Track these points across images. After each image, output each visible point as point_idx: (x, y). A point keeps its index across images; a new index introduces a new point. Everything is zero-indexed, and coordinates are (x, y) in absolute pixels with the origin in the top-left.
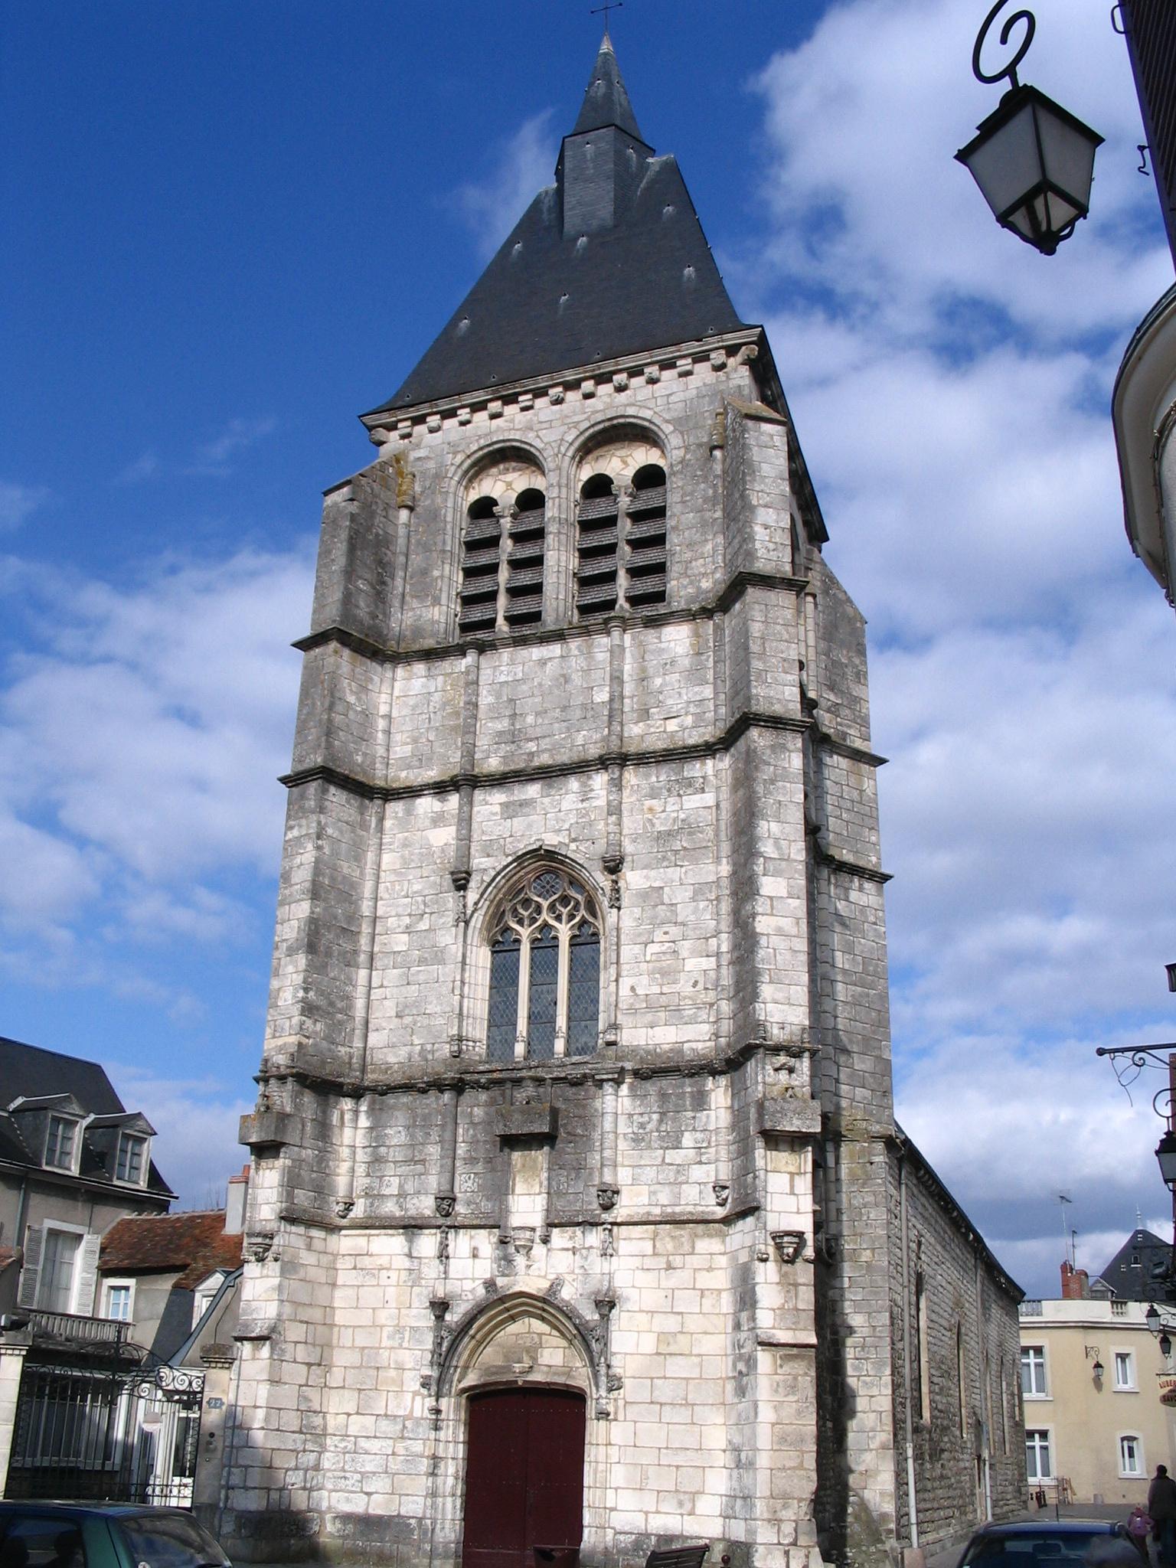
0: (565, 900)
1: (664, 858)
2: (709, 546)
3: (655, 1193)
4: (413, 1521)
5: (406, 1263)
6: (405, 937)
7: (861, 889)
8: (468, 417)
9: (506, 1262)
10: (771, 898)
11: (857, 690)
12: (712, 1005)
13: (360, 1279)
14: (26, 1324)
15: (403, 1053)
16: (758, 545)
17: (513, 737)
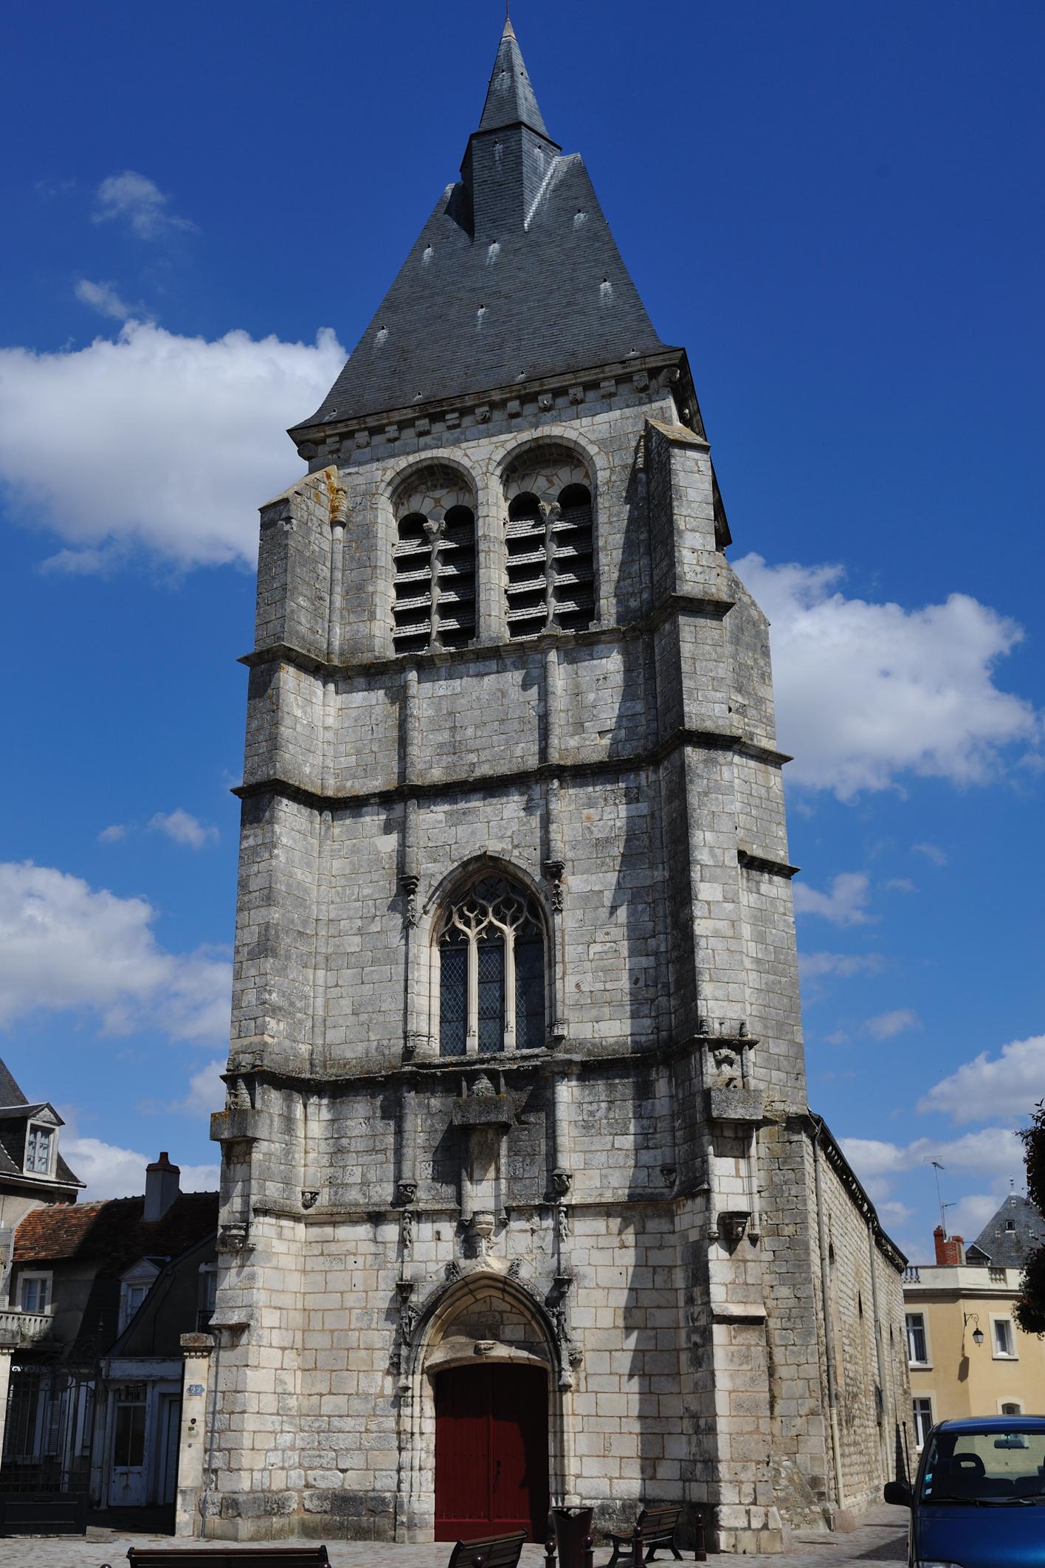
0: (508, 903)
1: (603, 864)
2: (636, 567)
3: (606, 1176)
4: (388, 1495)
5: (372, 1248)
6: (357, 939)
7: (770, 882)
8: (396, 434)
9: (470, 1249)
10: (708, 903)
11: (762, 691)
12: (653, 1001)
13: (327, 1265)
14: (1004, 1349)
15: (360, 1049)
16: (686, 569)
17: (454, 748)
